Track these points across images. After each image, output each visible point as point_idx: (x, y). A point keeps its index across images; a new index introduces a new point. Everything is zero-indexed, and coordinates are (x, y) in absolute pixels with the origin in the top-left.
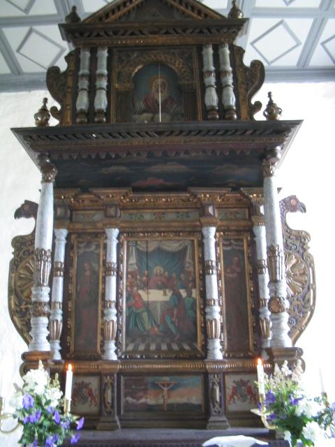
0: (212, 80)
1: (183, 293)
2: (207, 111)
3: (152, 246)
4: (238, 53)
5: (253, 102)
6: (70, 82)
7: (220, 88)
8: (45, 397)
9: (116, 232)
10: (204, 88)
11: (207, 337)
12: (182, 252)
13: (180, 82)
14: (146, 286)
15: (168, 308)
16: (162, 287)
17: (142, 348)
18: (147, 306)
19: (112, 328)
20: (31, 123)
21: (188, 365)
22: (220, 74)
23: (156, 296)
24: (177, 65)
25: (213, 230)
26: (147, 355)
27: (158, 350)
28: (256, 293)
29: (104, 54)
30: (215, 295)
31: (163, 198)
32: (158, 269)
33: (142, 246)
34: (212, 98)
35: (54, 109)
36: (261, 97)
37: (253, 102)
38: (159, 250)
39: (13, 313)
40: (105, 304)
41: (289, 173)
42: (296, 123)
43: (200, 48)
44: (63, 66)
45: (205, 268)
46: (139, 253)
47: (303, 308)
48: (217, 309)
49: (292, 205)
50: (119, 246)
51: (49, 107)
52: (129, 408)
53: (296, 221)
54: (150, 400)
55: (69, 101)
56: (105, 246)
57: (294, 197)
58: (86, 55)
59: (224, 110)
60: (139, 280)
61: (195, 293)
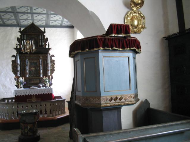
0: (41, 41)
1: (37, 68)
2: (40, 45)
3: (32, 62)
4: (45, 36)
5: (46, 38)
6: (21, 40)
7: (42, 42)
8: (23, 79)
9: (27, 60)
10: (39, 42)
11: (40, 74)
12: (37, 63)
13: (45, 78)
14: (32, 67)
15: (35, 70)
16: (34, 67)
17: (31, 75)
18: (32, 70)
19: (27, 73)
20: (16, 47)
21: (37, 78)
22: (42, 40)
23: (33, 69)
24: (36, 38)
25: (41, 60)
26: (32, 76)
27: (33, 76)
28: (26, 68)
29: (25, 36)
30: (41, 69)
31: (34, 55)
32: (33, 65)
33: (31, 62)
34: (41, 44)
35: (18, 44)
36: (47, 43)
37: (46, 38)
38: (33, 62)
39: (13, 71)
40: (26, 70)
41: (51, 52)
42: (51, 48)
43: (39, 35)
44: (19, 37)
45: (40, 65)
46: (31, 63)
47: (53, 70)
48: (41, 70)
49: (53, 56)
50: (28, 62)
51: (18, 44)
52: (30, 83)
53: (53, 58)
54: (33, 82)
55: (20, 43)
56: (26, 62)
57: (53, 55)
58: (23, 36)
59: (42, 45)
60: (30, 67)
61: (38, 68)
